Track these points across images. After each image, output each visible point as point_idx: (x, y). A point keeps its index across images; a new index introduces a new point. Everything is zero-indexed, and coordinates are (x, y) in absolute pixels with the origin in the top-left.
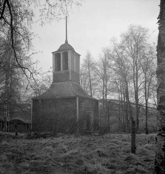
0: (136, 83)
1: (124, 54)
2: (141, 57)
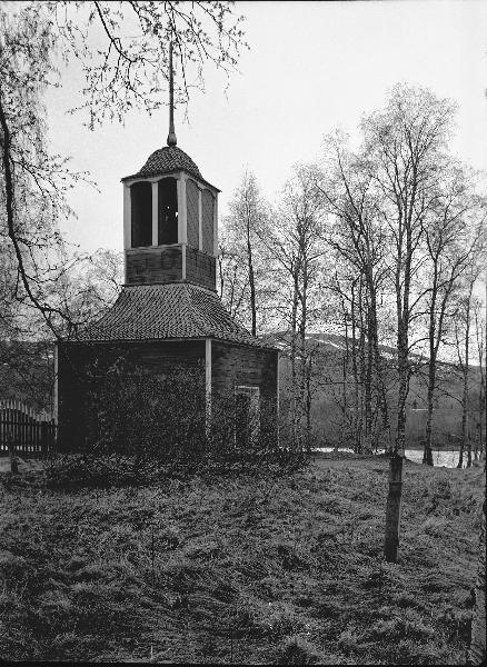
0: (402, 293)
1: (372, 191)
2: (426, 205)
